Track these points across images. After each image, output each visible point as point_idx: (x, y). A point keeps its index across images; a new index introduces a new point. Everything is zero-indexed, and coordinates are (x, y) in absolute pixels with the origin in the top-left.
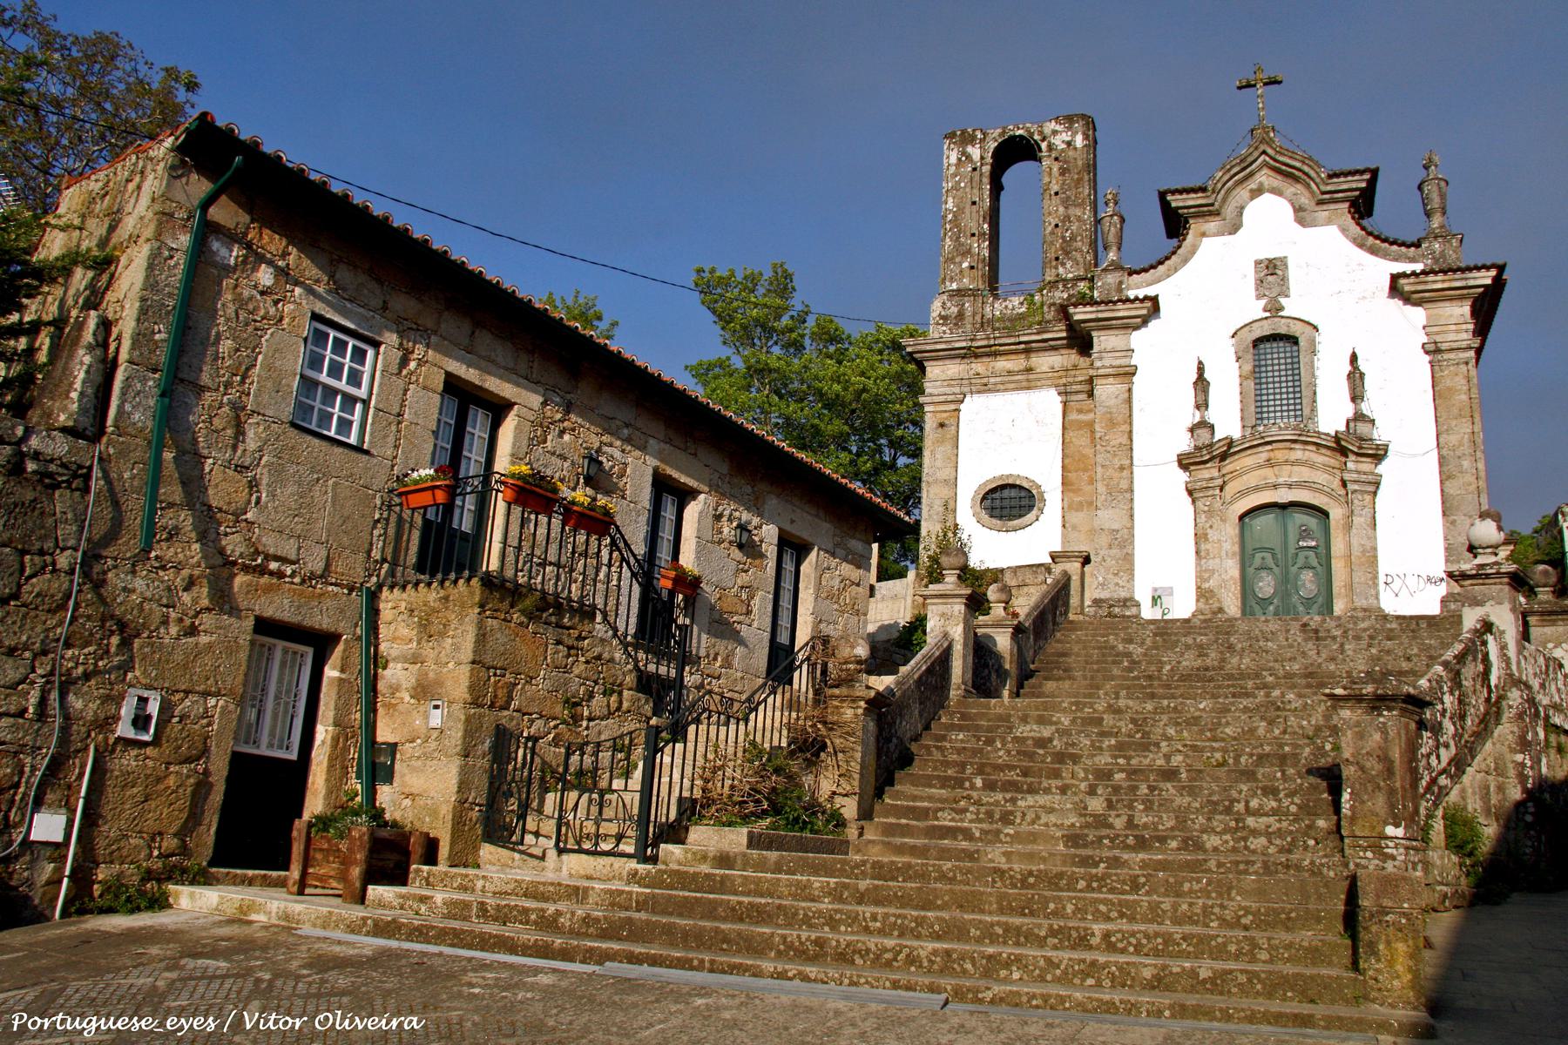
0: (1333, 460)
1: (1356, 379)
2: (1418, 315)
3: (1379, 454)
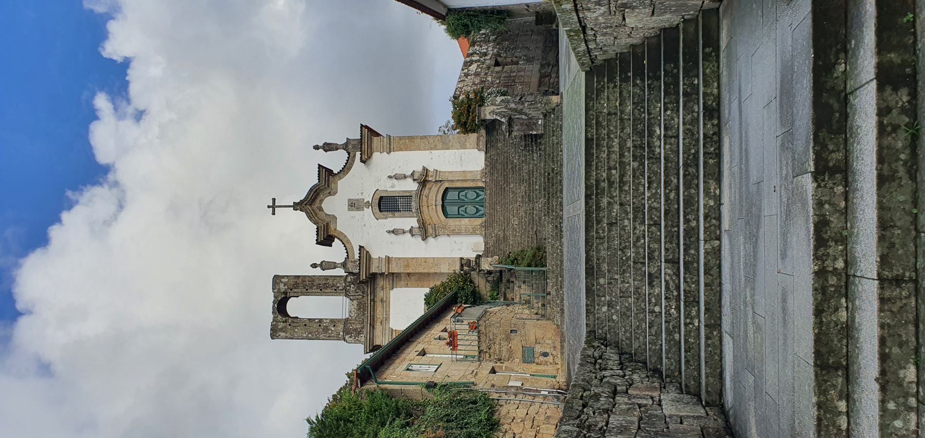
0: (428, 186)
1: (397, 177)
2: (376, 155)
3: (426, 170)
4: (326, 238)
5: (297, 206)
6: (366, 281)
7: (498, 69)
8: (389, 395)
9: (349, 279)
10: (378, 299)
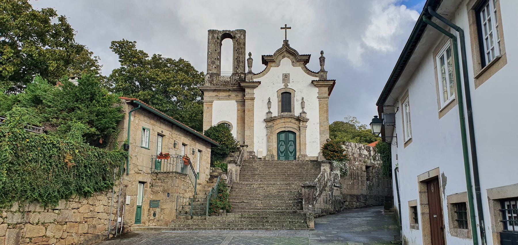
0: (297, 122)
1: (303, 103)
2: (316, 90)
3: (307, 120)
4: (266, 61)
5: (286, 42)
6: (240, 86)
7: (364, 168)
8: (119, 122)
9: (242, 75)
10: (230, 93)
